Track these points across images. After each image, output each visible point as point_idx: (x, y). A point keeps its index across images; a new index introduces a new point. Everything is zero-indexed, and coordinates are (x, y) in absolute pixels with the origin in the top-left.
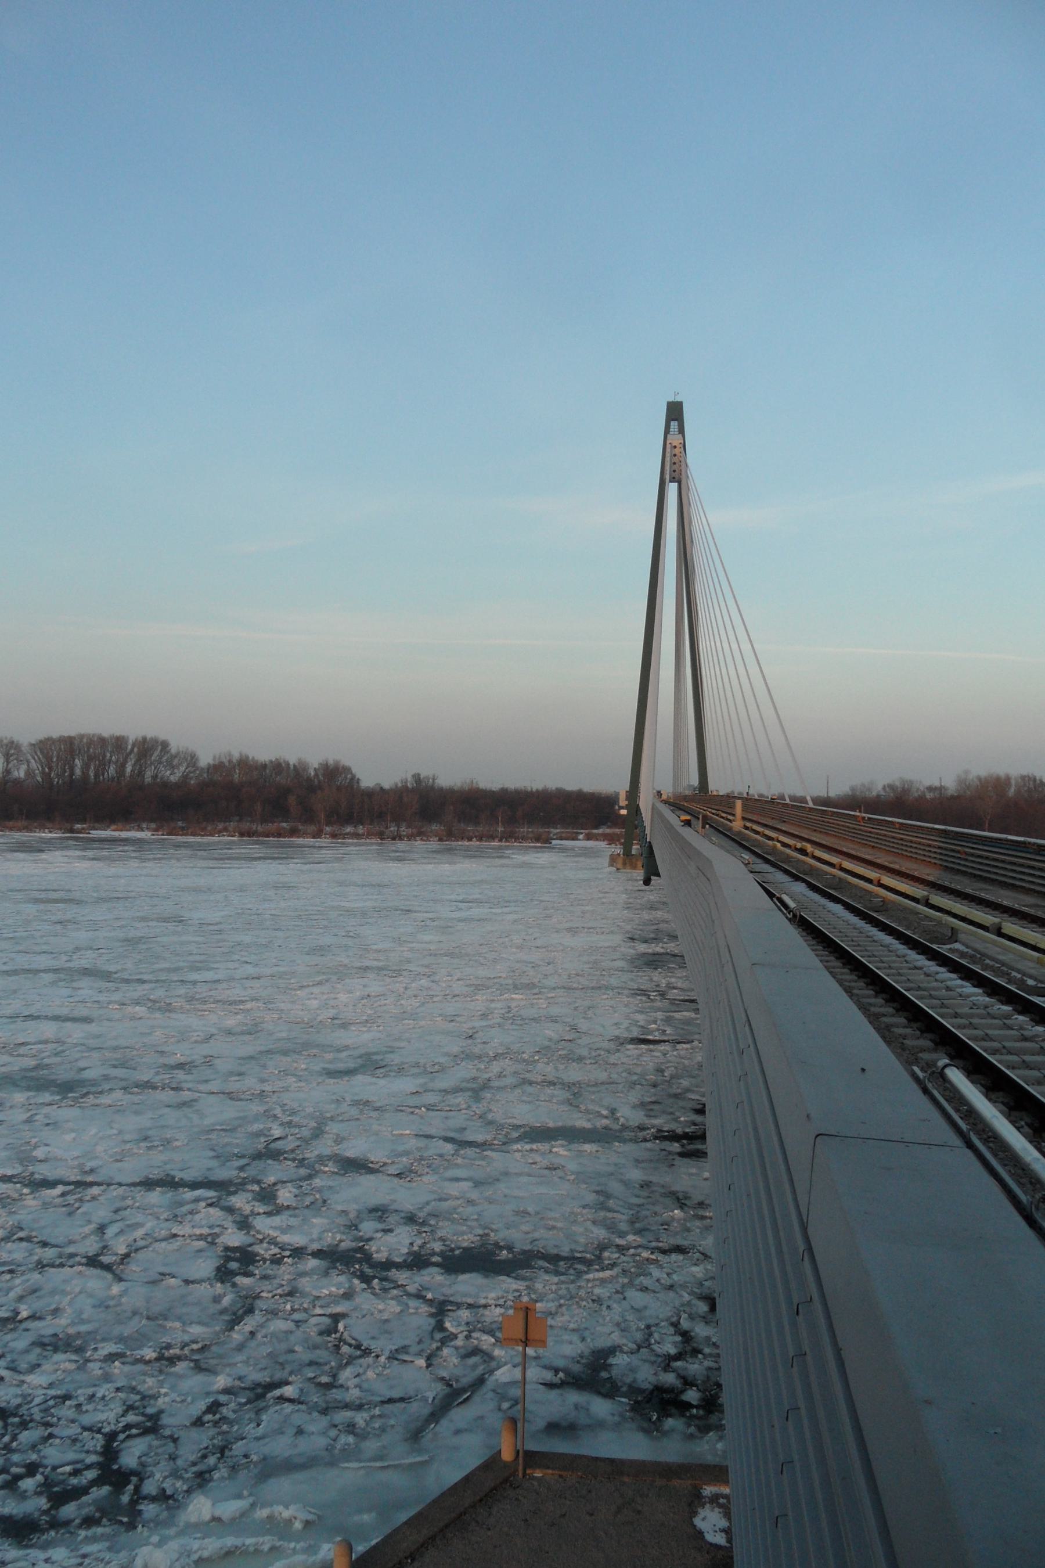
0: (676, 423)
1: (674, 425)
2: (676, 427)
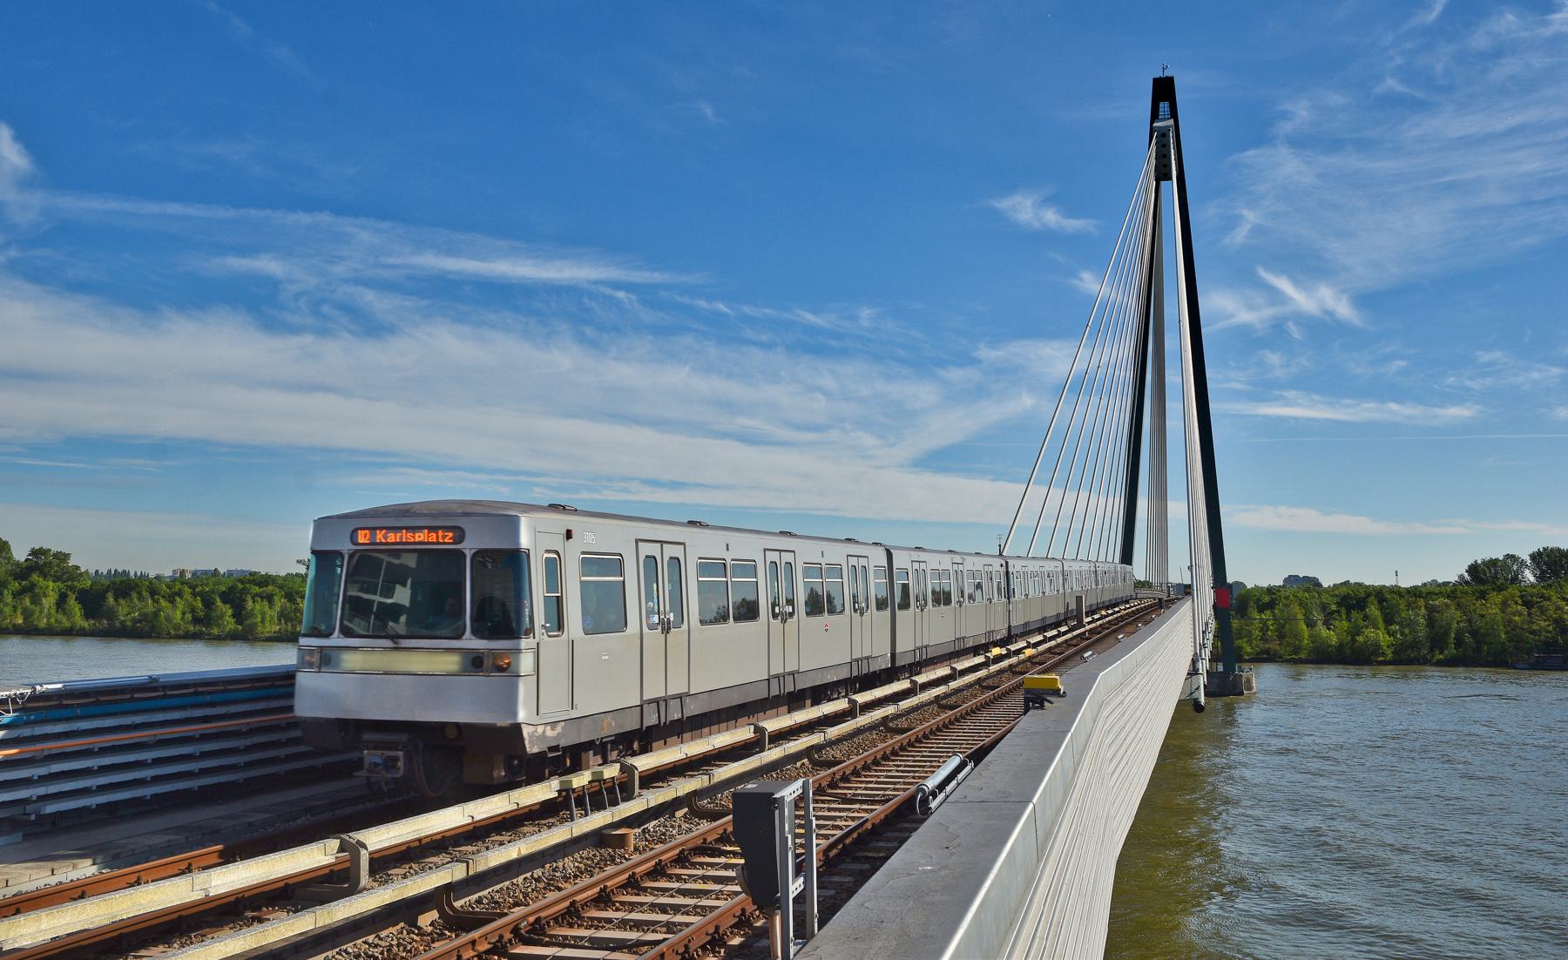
0: (1167, 104)
1: (1164, 107)
2: (1167, 109)
